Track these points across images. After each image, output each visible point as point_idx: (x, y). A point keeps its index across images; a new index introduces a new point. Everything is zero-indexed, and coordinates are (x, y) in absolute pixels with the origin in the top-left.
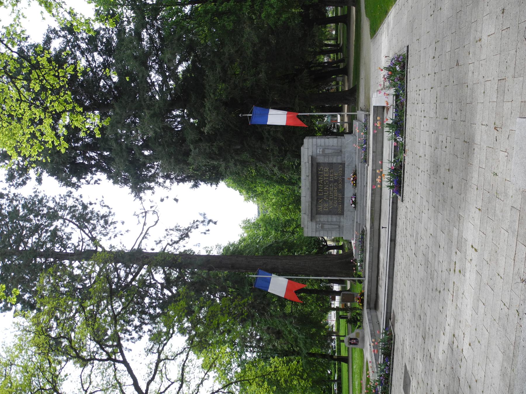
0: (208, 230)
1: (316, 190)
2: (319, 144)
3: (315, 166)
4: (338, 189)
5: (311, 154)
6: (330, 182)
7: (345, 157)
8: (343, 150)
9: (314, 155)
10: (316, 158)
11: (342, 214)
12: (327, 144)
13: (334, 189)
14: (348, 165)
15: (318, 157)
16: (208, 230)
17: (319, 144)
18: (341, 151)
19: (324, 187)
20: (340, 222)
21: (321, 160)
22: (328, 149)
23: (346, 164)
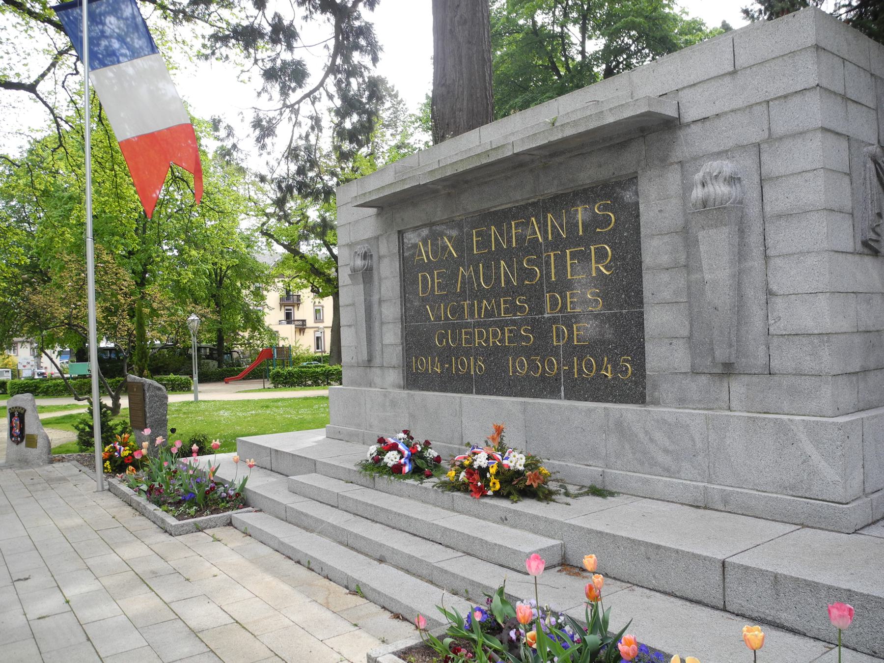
0: (242, 121)
1: (501, 204)
2: (773, 165)
3: (590, 172)
4: (505, 350)
5: (690, 114)
6: (535, 296)
7: (682, 402)
8: (738, 387)
9: (691, 142)
10: (664, 162)
11: (414, 380)
12: (783, 238)
13: (502, 325)
14: (621, 428)
15: (673, 178)
16: (242, 121)
17: (773, 165)
18: (728, 370)
19: (509, 254)
20: (382, 367)
21: (659, 203)
22: (741, 254)
23: (629, 411)
